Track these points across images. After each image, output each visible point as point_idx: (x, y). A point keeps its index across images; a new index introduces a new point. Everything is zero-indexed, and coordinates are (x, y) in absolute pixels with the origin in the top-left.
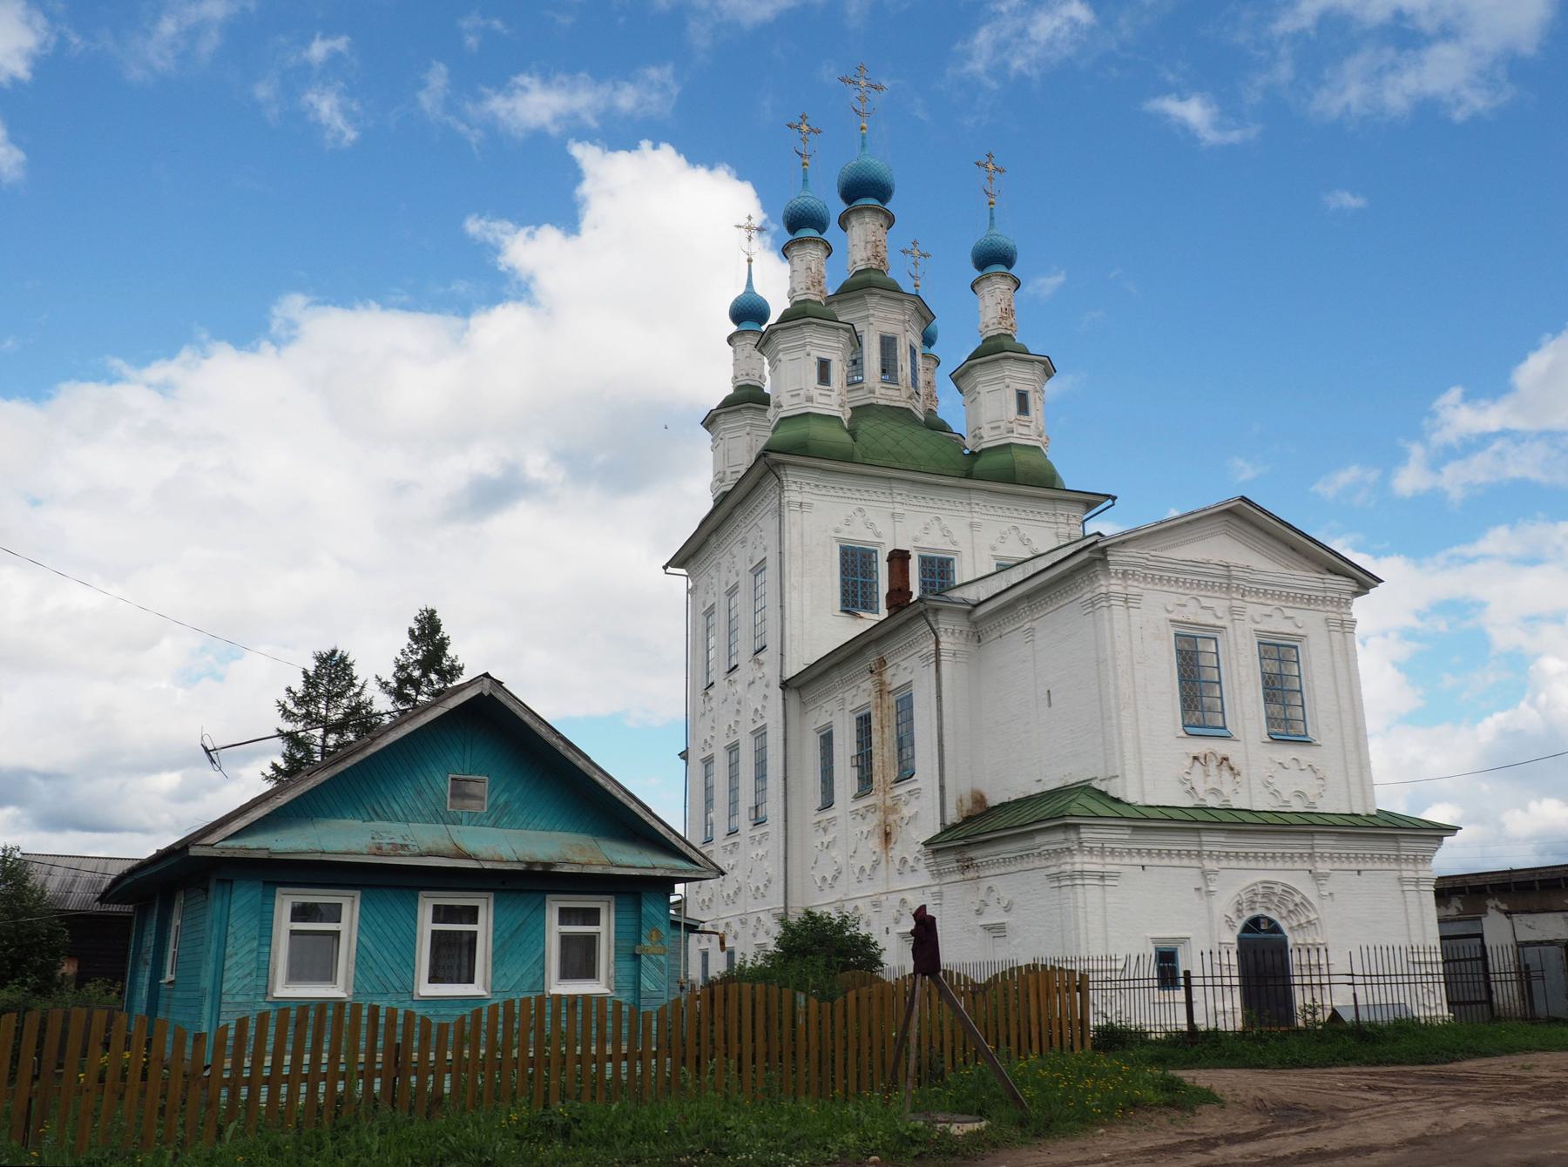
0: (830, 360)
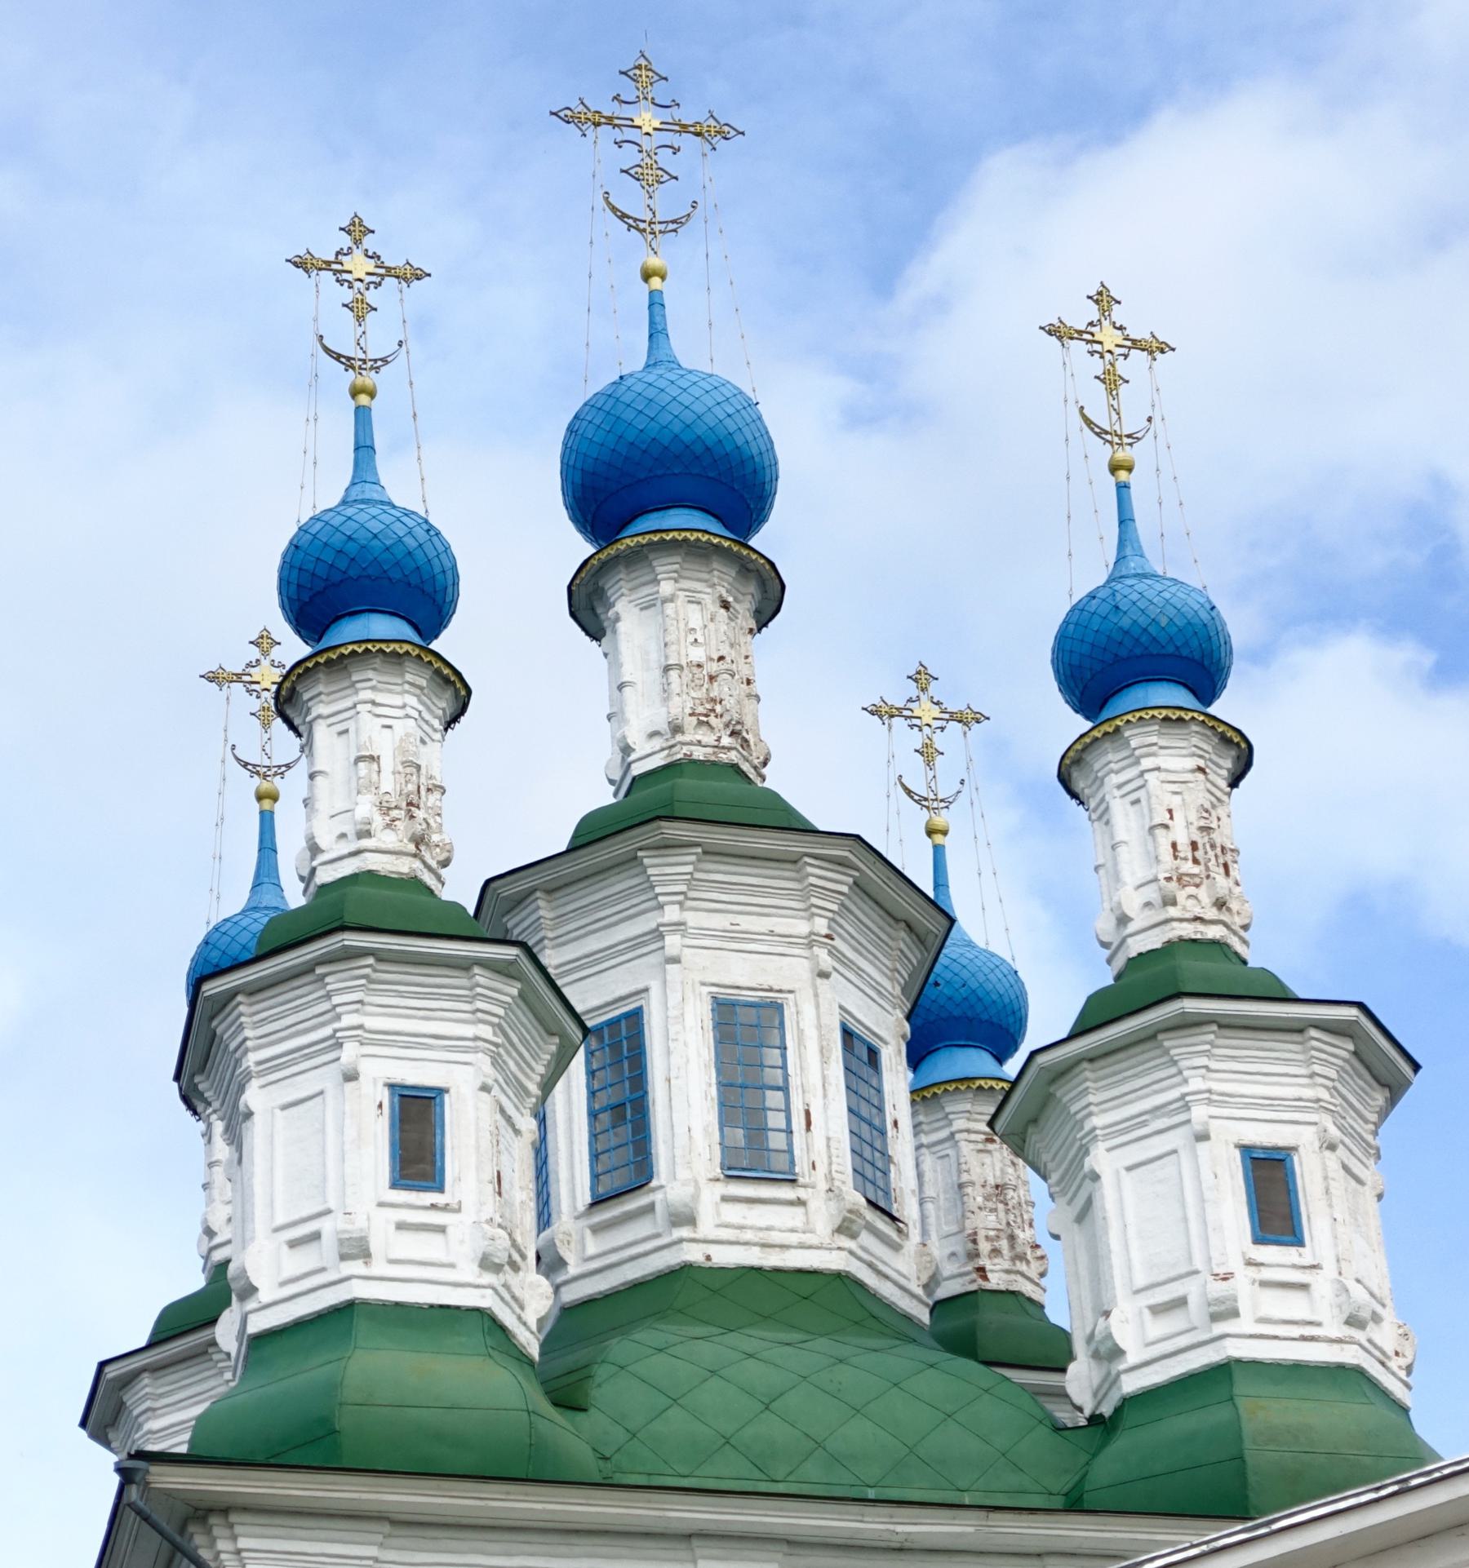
0: (442, 1091)
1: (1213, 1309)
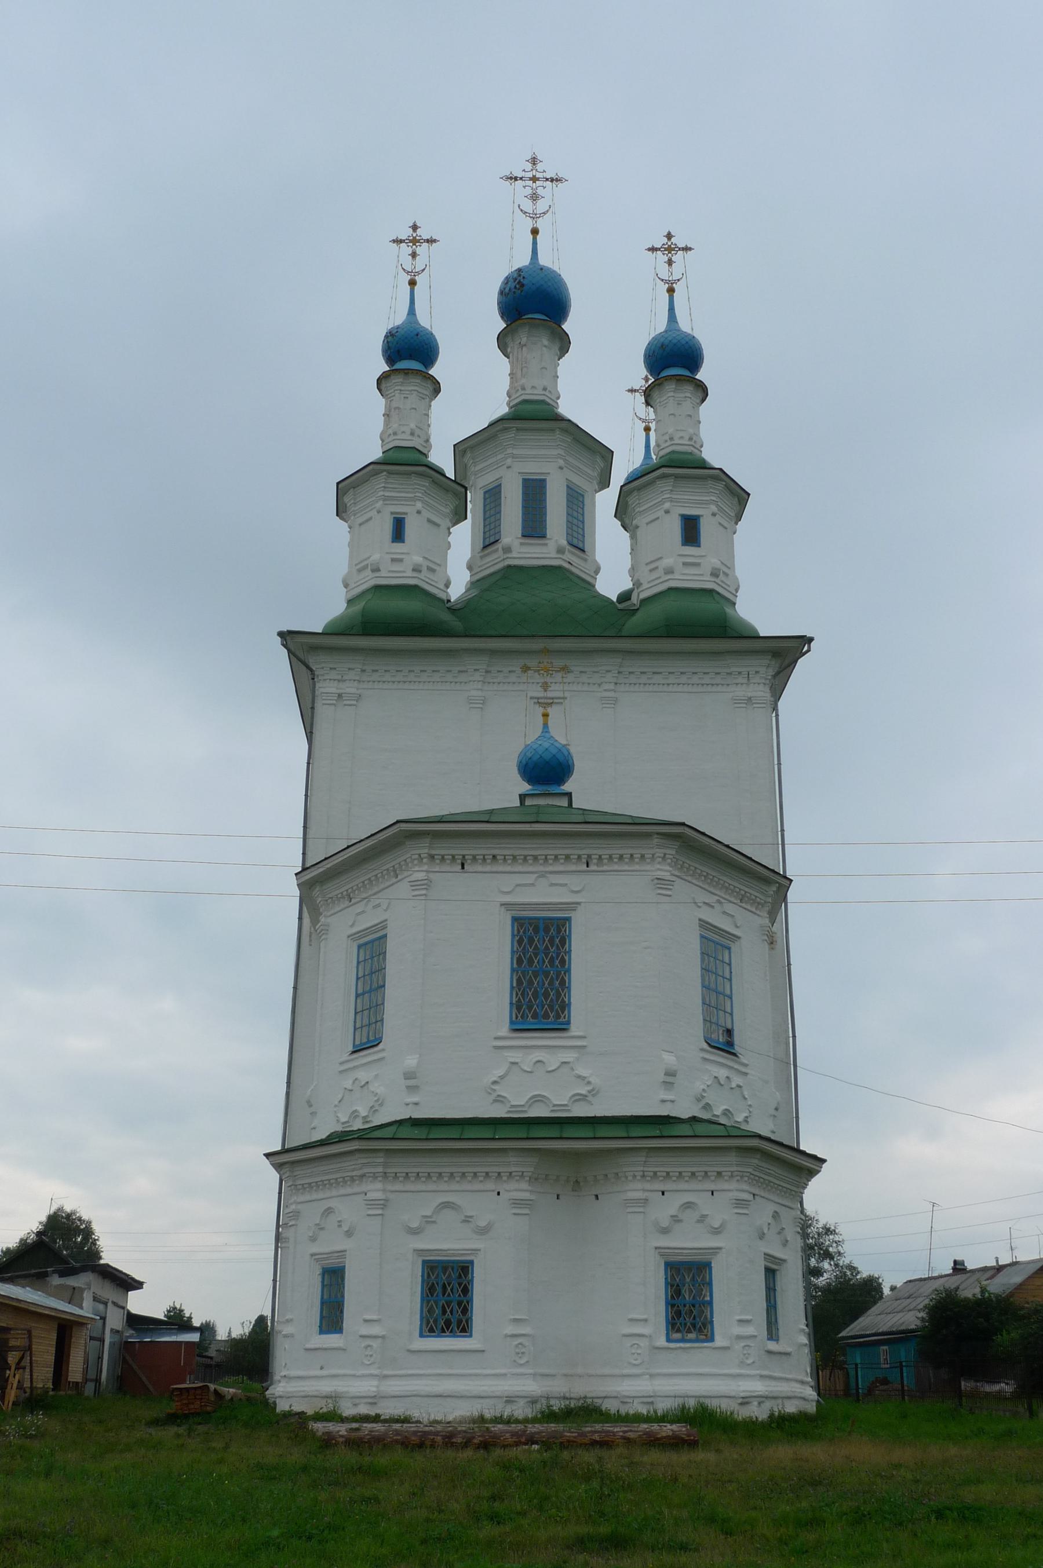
1: (358, 567)
